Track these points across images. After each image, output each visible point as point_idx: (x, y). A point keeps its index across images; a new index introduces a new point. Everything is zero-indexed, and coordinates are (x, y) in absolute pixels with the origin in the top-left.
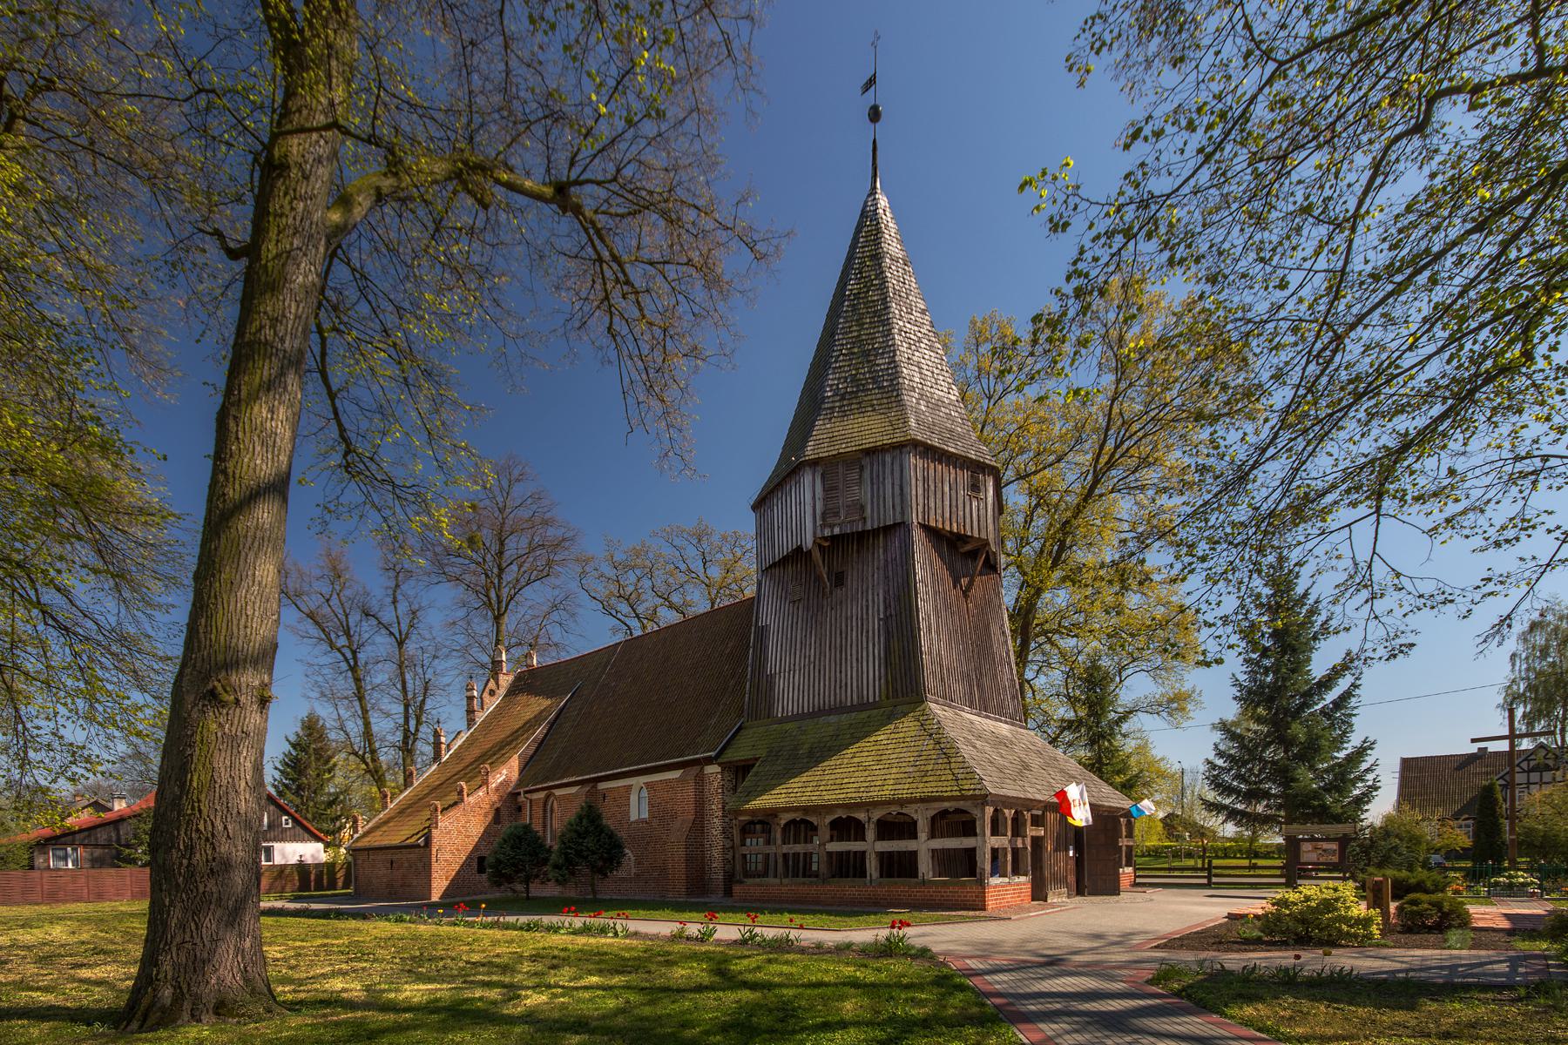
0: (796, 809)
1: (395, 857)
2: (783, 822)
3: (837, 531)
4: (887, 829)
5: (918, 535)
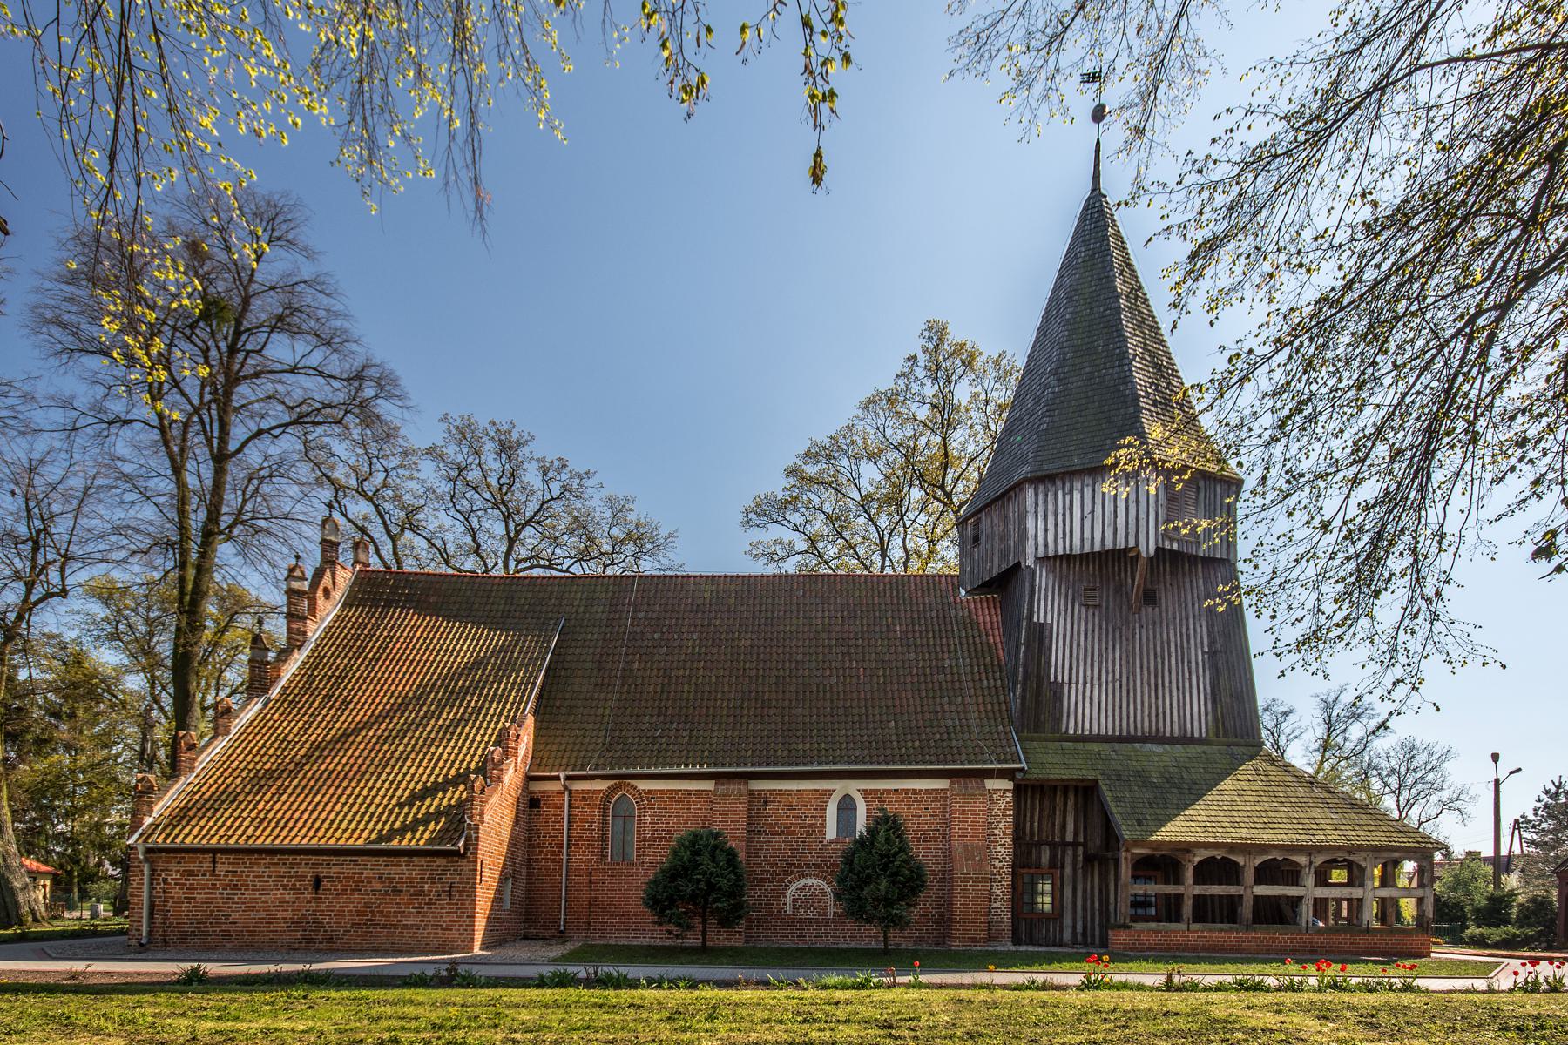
0: (1216, 846)
1: (323, 870)
2: (1197, 859)
3: (1175, 546)
4: (1266, 873)
5: (1042, 579)
